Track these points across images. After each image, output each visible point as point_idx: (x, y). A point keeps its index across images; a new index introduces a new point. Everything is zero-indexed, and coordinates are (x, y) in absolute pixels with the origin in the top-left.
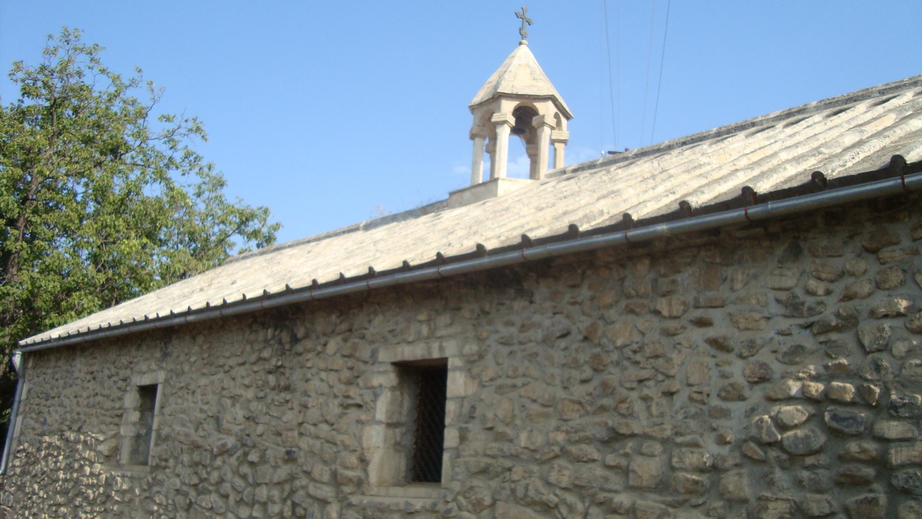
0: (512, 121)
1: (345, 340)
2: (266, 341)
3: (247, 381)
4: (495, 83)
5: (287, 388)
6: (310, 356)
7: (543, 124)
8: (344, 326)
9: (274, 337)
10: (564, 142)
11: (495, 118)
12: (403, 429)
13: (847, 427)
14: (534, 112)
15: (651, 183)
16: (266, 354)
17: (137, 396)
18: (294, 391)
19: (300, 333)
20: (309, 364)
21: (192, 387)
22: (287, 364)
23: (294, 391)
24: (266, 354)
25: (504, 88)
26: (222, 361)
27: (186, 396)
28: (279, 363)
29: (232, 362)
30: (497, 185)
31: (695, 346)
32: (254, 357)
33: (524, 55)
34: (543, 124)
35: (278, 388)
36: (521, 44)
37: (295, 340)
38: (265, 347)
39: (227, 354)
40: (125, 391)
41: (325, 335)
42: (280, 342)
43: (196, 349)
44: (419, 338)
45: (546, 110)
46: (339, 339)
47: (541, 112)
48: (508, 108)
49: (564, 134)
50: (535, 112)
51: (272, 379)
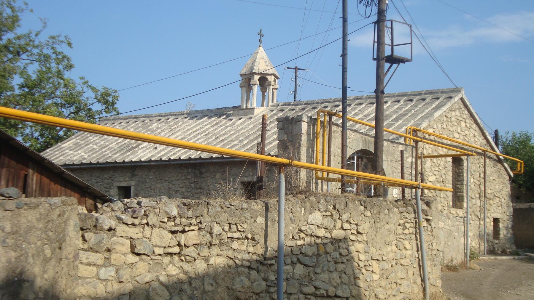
0: (258, 83)
1: (222, 174)
2: (188, 172)
3: (181, 186)
4: (250, 66)
5: (200, 188)
6: (209, 178)
7: (270, 85)
8: (221, 170)
9: (192, 172)
10: (276, 89)
11: (252, 82)
12: (6, 296)
13: (113, 139)
14: (267, 80)
15: (273, 214)
16: (189, 177)
17: (117, 190)
18: (203, 189)
19: (204, 171)
20: (208, 181)
21: (153, 187)
22: (199, 181)
23: (203, 189)
24: (189, 177)
25: (255, 70)
26: (167, 179)
27: (150, 191)
28: (196, 180)
29: (173, 179)
30: (254, 110)
31: (124, 212)
32: (183, 178)
33: (262, 53)
34: (270, 85)
35: (196, 188)
36: (260, 46)
37: (201, 173)
38: (188, 175)
39: (170, 176)
40: (110, 188)
41: (214, 172)
42: (195, 173)
43: (151, 173)
44: (249, 175)
45: (271, 79)
46: (220, 174)
47: (269, 80)
48: (257, 78)
49: (277, 86)
50: (267, 80)
51: (193, 185)
